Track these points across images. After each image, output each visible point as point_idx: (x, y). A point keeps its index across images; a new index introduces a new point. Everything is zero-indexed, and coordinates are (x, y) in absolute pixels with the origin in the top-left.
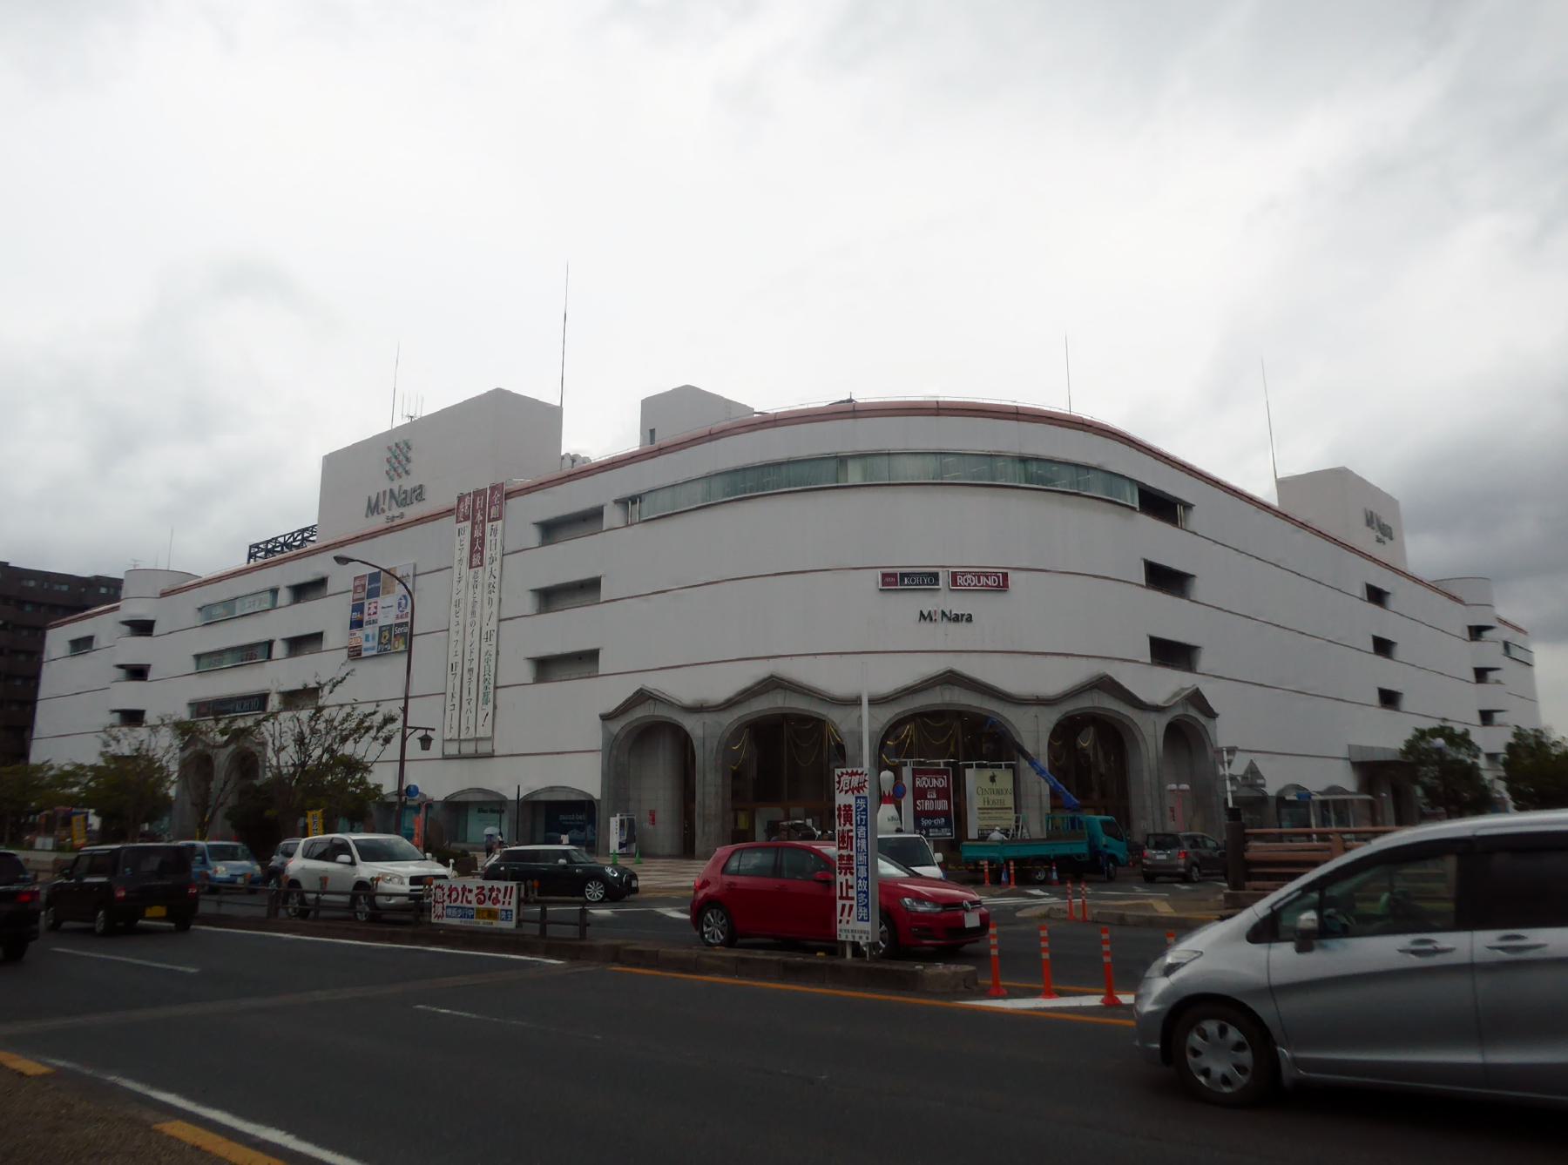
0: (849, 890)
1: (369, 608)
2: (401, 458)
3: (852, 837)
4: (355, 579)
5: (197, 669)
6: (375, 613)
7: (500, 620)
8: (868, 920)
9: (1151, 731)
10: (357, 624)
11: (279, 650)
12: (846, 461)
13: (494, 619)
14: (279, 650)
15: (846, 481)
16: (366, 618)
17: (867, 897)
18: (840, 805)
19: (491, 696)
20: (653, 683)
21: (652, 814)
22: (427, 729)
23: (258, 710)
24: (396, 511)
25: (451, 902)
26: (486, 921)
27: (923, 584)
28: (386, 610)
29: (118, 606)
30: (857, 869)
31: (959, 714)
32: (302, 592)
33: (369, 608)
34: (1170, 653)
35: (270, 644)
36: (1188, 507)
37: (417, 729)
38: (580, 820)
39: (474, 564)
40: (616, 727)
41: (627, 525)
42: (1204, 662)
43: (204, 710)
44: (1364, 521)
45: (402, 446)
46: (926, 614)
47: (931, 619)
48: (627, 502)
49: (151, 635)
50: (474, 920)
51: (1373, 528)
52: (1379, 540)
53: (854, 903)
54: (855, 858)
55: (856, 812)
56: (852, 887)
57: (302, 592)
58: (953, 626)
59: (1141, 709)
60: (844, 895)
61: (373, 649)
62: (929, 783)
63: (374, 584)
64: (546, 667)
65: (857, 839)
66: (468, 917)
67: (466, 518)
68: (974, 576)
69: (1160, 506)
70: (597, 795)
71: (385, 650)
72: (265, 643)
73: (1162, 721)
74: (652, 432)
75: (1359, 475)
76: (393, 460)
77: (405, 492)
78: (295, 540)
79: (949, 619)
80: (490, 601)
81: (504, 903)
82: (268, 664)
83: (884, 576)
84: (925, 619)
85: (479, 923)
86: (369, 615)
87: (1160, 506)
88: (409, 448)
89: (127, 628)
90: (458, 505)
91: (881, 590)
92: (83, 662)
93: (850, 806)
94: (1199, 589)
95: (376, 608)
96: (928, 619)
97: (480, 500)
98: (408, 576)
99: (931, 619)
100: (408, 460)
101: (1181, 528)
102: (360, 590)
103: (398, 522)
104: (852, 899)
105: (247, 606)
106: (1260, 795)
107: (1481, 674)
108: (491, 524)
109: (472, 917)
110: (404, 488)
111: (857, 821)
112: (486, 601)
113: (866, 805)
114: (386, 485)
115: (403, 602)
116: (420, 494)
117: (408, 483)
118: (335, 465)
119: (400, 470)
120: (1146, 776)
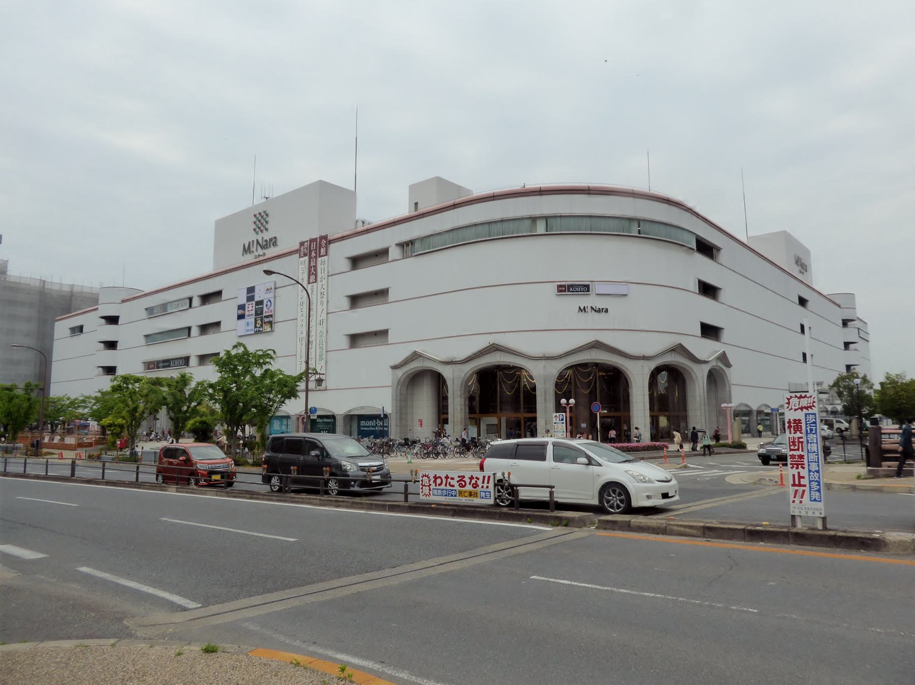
0: (801, 479)
1: (248, 308)
2: (262, 221)
3: (802, 442)
6: (252, 310)
7: (328, 313)
8: (820, 501)
9: (699, 375)
11: (195, 331)
12: (536, 220)
13: (325, 312)
14: (195, 331)
15: (536, 232)
16: (247, 313)
17: (819, 485)
18: (790, 420)
19: (324, 356)
20: (419, 348)
21: (421, 421)
23: (184, 365)
25: (436, 486)
27: (581, 291)
29: (98, 308)
30: (809, 465)
31: (598, 366)
32: (206, 299)
33: (248, 308)
34: (710, 331)
35: (189, 329)
36: (719, 249)
39: (311, 281)
40: (400, 373)
41: (404, 258)
43: (152, 366)
44: (794, 262)
45: (263, 214)
47: (585, 311)
48: (403, 245)
49: (117, 324)
51: (798, 265)
52: (801, 272)
53: (807, 489)
54: (806, 457)
55: (806, 424)
56: (803, 477)
57: (206, 299)
58: (596, 314)
59: (693, 360)
60: (797, 483)
61: (252, 330)
64: (355, 339)
65: (808, 444)
66: (452, 496)
67: (305, 255)
69: (706, 249)
70: (389, 410)
71: (259, 331)
72: (187, 327)
73: (706, 369)
74: (416, 204)
75: (796, 238)
76: (258, 223)
77: (266, 240)
79: (595, 311)
80: (322, 303)
81: (482, 487)
82: (189, 340)
83: (559, 286)
86: (249, 311)
87: (706, 249)
89: (103, 321)
90: (300, 248)
91: (557, 295)
93: (800, 420)
94: (722, 296)
96: (583, 311)
97: (313, 244)
98: (271, 288)
99: (585, 311)
100: (267, 222)
103: (261, 258)
104: (805, 486)
105: (175, 306)
106: (749, 409)
107: (847, 345)
108: (321, 258)
109: (455, 496)
110: (265, 239)
111: (807, 430)
112: (319, 303)
113: (815, 419)
114: (253, 237)
115: (269, 303)
116: (276, 242)
117: (267, 236)
118: (223, 226)
119: (262, 228)
120: (698, 398)
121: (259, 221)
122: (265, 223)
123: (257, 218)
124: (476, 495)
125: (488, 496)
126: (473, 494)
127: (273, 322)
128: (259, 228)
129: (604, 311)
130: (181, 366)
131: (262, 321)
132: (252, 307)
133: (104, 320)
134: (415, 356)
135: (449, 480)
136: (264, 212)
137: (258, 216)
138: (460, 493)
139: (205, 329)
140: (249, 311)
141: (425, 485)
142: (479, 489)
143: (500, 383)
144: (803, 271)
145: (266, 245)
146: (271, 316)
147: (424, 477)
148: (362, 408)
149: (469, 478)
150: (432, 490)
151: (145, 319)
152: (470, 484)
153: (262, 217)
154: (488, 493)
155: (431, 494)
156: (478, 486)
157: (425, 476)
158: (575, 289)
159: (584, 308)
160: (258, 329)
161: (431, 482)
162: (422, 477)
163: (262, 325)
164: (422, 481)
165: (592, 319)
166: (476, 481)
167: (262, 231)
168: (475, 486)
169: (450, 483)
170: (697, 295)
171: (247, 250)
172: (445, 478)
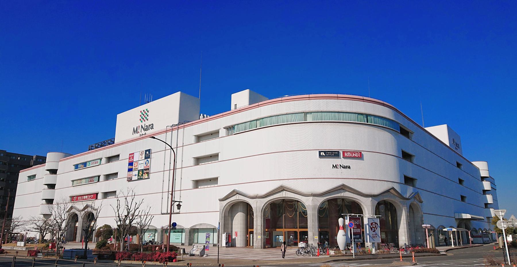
1: (135, 164)
2: (145, 115)
4: (130, 154)
5: (73, 185)
6: (137, 166)
10: (130, 170)
16: (134, 168)
22: (179, 202)
24: (143, 132)
32: (110, 159)
33: (135, 164)
37: (176, 201)
45: (145, 111)
47: (336, 167)
48: (230, 129)
49: (56, 174)
57: (110, 159)
62: (354, 223)
64: (197, 183)
68: (350, 153)
70: (217, 226)
77: (147, 126)
89: (48, 172)
95: (137, 164)
96: (335, 167)
99: (336, 167)
101: (410, 140)
105: (91, 164)
114: (140, 124)
115: (147, 162)
116: (153, 126)
117: (147, 123)
119: (145, 119)
121: (143, 115)
127: (149, 173)
128: (143, 119)
129: (347, 167)
131: (142, 172)
132: (137, 164)
134: (234, 193)
136: (147, 110)
137: (143, 112)
139: (108, 177)
146: (148, 169)
148: (201, 224)
153: (145, 112)
159: (336, 165)
160: (140, 177)
167: (144, 121)
171: (135, 131)
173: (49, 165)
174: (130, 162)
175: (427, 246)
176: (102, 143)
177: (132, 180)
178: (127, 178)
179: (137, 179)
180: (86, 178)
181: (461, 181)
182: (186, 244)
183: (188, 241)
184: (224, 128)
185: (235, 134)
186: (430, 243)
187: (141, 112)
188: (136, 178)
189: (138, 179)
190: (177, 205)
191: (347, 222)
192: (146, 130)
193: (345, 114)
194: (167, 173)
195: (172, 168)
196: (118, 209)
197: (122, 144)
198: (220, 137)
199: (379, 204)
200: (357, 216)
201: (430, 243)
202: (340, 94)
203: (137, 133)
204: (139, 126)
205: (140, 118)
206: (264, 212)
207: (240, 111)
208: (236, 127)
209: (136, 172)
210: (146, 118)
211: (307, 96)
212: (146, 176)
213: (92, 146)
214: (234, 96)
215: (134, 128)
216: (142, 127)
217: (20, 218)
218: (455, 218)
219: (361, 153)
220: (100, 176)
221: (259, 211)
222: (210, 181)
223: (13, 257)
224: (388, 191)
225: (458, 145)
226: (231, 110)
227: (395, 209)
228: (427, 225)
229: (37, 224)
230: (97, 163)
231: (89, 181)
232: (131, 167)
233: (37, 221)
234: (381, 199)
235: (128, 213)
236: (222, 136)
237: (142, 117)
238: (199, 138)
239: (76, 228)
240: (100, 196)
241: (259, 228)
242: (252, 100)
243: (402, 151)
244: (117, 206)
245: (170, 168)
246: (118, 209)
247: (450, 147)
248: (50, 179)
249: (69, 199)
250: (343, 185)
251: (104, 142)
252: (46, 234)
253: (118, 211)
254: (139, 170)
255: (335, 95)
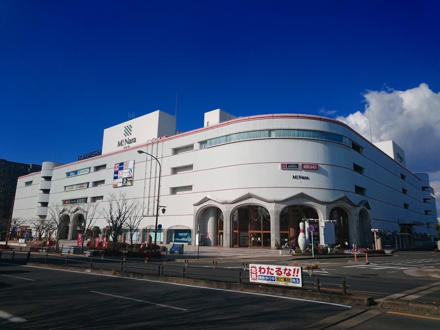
1: (120, 173)
2: (129, 130)
4: (115, 164)
6: (121, 174)
16: (119, 176)
22: (164, 207)
25: (261, 273)
26: (283, 283)
27: (294, 168)
28: (124, 174)
32: (97, 168)
33: (120, 173)
34: (359, 190)
36: (363, 148)
37: (161, 207)
38: (185, 235)
40: (198, 207)
42: (367, 193)
46: (295, 176)
48: (203, 143)
50: (276, 282)
52: (400, 162)
57: (97, 168)
63: (121, 166)
64: (174, 190)
66: (272, 280)
68: (309, 166)
76: (126, 131)
77: (130, 140)
78: (92, 154)
81: (294, 276)
83: (282, 165)
84: (294, 178)
85: (279, 283)
86: (120, 175)
88: (131, 127)
92: (29, 188)
95: (122, 173)
96: (295, 178)
99: (296, 178)
100: (131, 131)
102: (117, 168)
109: (275, 280)
114: (124, 138)
115: (131, 171)
116: (135, 140)
117: (131, 137)
119: (128, 133)
121: (127, 130)
122: (130, 131)
123: (126, 129)
124: (289, 280)
125: (298, 281)
126: (287, 280)
127: (132, 180)
128: (127, 133)
129: (306, 178)
130: (83, 202)
131: (126, 180)
132: (122, 173)
133: (44, 178)
134: (206, 199)
135: (270, 270)
136: (130, 126)
137: (126, 127)
138: (278, 279)
139: (96, 184)
140: (120, 175)
141: (253, 273)
142: (291, 277)
143: (250, 214)
144: (401, 161)
145: (130, 142)
146: (131, 177)
147: (253, 268)
148: (177, 226)
149: (284, 270)
150: (258, 276)
151: (65, 178)
152: (285, 273)
153: (128, 128)
154: (298, 280)
155: (258, 279)
156: (291, 275)
157: (253, 267)
158: (291, 166)
159: (296, 176)
160: (124, 184)
161: (258, 271)
162: (251, 268)
163: (126, 182)
164: (251, 270)
165: (299, 183)
166: (289, 272)
167: (128, 135)
168: (289, 274)
169: (270, 272)
170: (353, 171)
171: (120, 144)
172: (267, 269)
173: (43, 173)
174: (115, 171)
175: (375, 248)
176: (90, 154)
177: (118, 186)
178: (113, 185)
179: (121, 186)
180: (77, 185)
181: (404, 191)
182: (164, 242)
183: (165, 240)
184: (198, 142)
185: (207, 148)
186: (378, 245)
187: (125, 127)
188: (120, 185)
189: (122, 186)
190: (162, 210)
191: (307, 225)
192: (129, 143)
193: (289, 131)
194: (153, 180)
195: (158, 175)
196: (111, 212)
197: (109, 155)
198: (194, 150)
199: (333, 210)
200: (316, 221)
201: (378, 245)
202: (300, 113)
203: (121, 146)
204: (123, 140)
205: (124, 133)
206: (232, 215)
207: (212, 128)
208: (208, 142)
209: (121, 180)
210: (129, 133)
211: (271, 115)
212: (129, 183)
213: (81, 156)
214: (206, 114)
215: (119, 141)
216: (126, 140)
217: (20, 218)
218: (398, 223)
219: (317, 165)
220: (89, 182)
221: (228, 214)
222: (185, 188)
223: (27, 253)
224: (341, 199)
225: (402, 158)
226: (204, 127)
227: (347, 214)
228: (376, 230)
229: (35, 224)
230: (87, 171)
231: (80, 187)
232: (116, 175)
233: (35, 221)
234: (334, 205)
235: (120, 216)
236: (196, 149)
237: (126, 132)
238: (176, 151)
239: (68, 228)
240: (89, 200)
241: (228, 230)
242: (222, 119)
243: (353, 164)
244: (110, 210)
245: (146, 176)
246: (111, 212)
247: (395, 160)
248: (45, 185)
249: (61, 203)
250: (249, 194)
251: (92, 153)
252: (43, 232)
253: (111, 213)
254: (123, 178)
255: (296, 115)
